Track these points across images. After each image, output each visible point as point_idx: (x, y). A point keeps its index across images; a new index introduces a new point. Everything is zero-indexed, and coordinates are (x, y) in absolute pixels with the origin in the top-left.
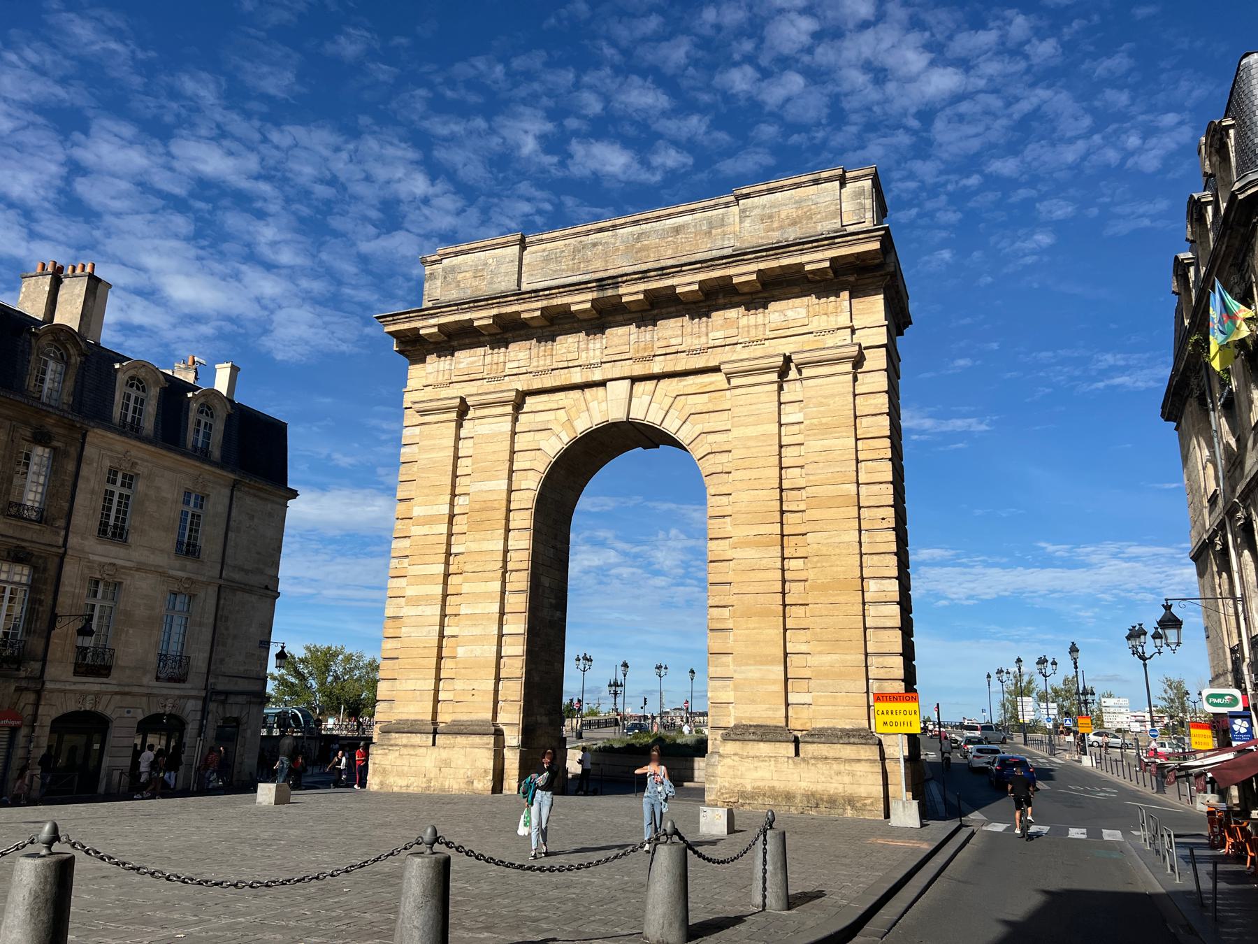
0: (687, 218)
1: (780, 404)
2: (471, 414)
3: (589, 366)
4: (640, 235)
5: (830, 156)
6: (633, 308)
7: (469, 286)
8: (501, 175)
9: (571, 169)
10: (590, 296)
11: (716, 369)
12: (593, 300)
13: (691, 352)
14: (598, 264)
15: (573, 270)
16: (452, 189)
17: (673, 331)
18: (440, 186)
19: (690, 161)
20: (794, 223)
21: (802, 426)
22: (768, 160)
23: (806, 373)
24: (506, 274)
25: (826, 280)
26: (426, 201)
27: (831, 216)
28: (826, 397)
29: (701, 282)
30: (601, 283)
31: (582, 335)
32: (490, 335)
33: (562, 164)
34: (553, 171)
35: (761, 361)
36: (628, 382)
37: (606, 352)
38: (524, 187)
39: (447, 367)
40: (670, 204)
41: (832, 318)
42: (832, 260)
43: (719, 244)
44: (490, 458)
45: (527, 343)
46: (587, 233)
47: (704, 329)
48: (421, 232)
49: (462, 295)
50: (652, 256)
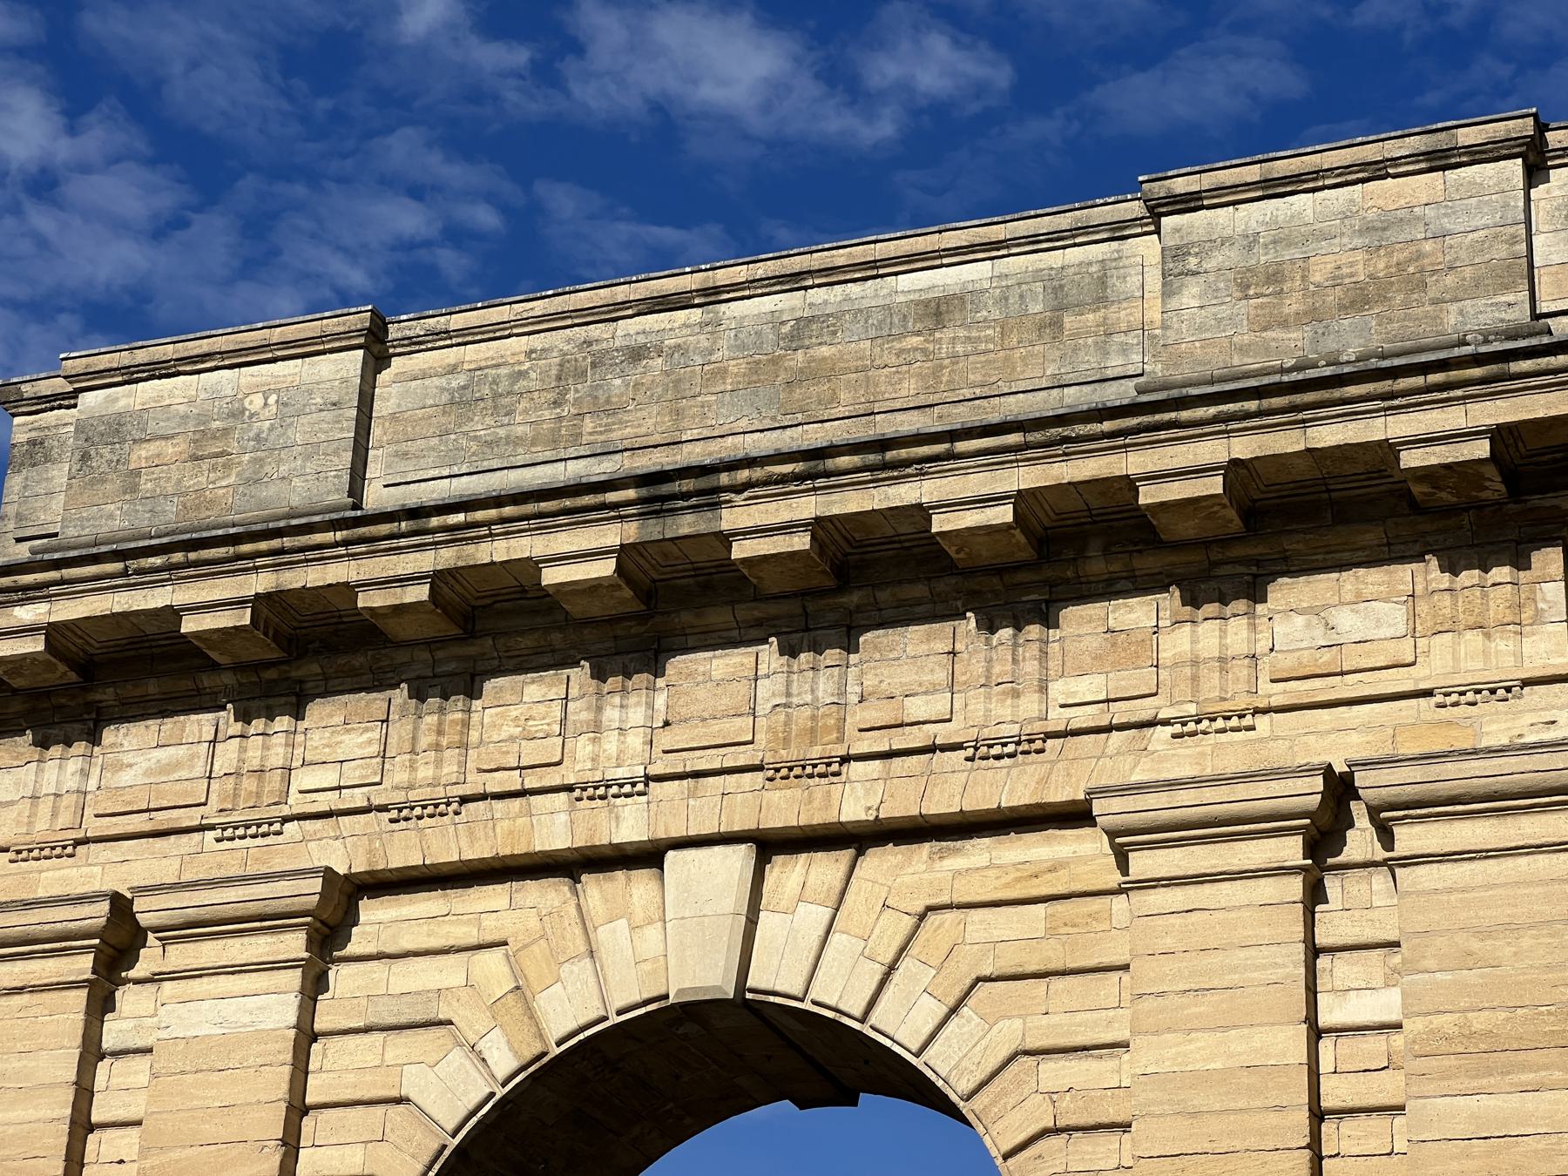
0: (976, 273)
1: (1314, 952)
2: (149, 960)
3: (601, 790)
4: (804, 324)
5: (1504, 71)
6: (771, 582)
7: (173, 487)
8: (323, 104)
9: (576, 89)
10: (611, 535)
11: (1076, 815)
12: (624, 552)
13: (981, 750)
14: (647, 422)
15: (554, 442)
16: (141, 146)
17: (916, 671)
18: (96, 138)
19: (1001, 76)
20: (1359, 299)
21: (1398, 1040)
22: (1274, 76)
23: (1409, 838)
24: (311, 450)
25: (1480, 506)
26: (44, 184)
27: (1494, 280)
28: (1484, 934)
29: (1022, 499)
30: (657, 491)
31: (400, 695)
32: (239, 668)
33: (545, 74)
34: (512, 96)
35: (1241, 791)
36: (740, 858)
37: (666, 740)
38: (404, 148)
39: (71, 783)
40: (921, 220)
41: (1503, 645)
42: (1500, 435)
43: (1088, 363)
44: (209, 1130)
45: (374, 702)
46: (612, 313)
47: (1030, 667)
48: (21, 292)
49: (143, 521)
50: (847, 400)
